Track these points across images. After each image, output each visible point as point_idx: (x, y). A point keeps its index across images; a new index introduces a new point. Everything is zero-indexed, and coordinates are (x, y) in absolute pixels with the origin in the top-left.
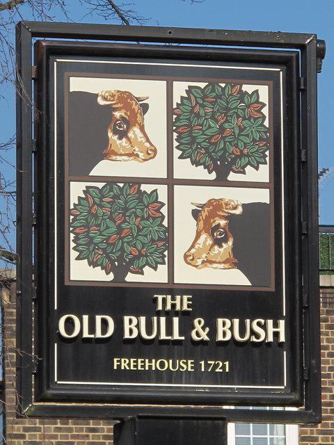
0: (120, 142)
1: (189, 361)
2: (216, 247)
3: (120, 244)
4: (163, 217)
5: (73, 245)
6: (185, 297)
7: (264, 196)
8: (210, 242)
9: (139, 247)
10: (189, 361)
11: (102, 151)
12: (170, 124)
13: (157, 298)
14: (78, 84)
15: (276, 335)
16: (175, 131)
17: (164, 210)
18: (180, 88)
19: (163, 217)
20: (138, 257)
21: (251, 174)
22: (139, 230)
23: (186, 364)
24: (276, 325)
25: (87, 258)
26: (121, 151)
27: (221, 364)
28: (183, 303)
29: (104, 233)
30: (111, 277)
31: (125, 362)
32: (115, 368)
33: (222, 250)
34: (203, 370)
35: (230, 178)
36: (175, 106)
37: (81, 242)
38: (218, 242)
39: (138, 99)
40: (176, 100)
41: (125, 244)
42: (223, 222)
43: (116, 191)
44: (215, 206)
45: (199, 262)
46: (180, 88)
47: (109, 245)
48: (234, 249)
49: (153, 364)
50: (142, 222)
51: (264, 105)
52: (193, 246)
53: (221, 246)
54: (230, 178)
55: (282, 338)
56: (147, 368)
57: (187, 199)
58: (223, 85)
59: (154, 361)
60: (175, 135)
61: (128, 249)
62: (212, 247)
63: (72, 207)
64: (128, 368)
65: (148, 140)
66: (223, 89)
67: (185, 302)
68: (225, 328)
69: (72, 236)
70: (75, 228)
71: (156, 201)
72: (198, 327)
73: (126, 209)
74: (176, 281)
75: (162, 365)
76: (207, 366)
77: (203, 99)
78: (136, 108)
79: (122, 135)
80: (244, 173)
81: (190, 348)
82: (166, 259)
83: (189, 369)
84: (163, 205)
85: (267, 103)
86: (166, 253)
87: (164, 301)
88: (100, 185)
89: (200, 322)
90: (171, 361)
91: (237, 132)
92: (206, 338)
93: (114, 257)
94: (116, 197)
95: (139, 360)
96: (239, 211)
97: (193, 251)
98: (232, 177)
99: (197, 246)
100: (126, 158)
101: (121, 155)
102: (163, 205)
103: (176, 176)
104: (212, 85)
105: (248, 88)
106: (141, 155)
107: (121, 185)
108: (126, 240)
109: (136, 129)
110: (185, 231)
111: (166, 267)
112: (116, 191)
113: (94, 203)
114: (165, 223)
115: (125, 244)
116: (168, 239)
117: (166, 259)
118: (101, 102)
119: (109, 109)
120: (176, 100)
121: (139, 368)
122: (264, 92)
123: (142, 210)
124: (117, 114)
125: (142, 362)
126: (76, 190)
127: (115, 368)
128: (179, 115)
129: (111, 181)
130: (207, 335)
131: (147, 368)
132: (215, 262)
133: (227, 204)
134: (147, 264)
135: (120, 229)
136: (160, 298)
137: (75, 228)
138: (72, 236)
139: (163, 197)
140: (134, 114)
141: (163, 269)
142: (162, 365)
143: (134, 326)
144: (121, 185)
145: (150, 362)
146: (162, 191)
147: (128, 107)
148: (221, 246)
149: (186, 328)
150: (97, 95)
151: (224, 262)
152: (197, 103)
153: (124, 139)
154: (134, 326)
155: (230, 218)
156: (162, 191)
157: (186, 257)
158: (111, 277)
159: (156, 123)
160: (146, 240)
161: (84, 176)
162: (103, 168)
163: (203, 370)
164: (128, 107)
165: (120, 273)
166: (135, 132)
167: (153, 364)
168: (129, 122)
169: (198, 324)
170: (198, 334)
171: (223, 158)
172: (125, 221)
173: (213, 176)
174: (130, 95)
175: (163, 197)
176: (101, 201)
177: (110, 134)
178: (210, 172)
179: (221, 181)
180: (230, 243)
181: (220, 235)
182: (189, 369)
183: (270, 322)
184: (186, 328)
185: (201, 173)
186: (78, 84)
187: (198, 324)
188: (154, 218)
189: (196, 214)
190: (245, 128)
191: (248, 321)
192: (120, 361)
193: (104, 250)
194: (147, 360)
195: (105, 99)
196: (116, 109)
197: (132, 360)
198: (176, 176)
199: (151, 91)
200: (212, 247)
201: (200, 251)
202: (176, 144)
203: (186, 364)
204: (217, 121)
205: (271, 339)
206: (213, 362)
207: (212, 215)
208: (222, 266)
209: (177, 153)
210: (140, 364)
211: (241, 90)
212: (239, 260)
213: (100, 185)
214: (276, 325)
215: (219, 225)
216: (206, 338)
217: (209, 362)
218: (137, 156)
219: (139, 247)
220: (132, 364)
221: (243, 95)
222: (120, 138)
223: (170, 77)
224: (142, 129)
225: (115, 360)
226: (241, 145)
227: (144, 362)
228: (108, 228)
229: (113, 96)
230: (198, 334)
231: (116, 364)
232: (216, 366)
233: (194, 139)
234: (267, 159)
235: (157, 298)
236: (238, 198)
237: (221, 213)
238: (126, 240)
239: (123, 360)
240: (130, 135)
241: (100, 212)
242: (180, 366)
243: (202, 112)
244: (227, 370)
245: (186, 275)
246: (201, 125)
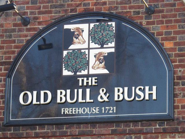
0: (76, 40)
1: (97, 108)
3: (76, 65)
4: (87, 58)
5: (64, 66)
6: (94, 78)
7: (113, 50)
8: (99, 63)
9: (80, 66)
10: (97, 108)
11: (71, 42)
12: (89, 34)
13: (163, 43)
15: (150, 95)
16: (90, 36)
17: (87, 56)
19: (87, 58)
20: (80, 68)
21: (110, 45)
22: (81, 61)
23: (95, 109)
24: (151, 89)
25: (67, 69)
26: (77, 42)
27: (112, 108)
28: (93, 81)
29: (72, 63)
30: (73, 74)
31: (67, 110)
32: (62, 113)
33: (102, 65)
34: (103, 112)
35: (104, 46)
36: (90, 30)
37: (66, 66)
38: (101, 63)
39: (81, 29)
40: (91, 28)
41: (77, 65)
42: (102, 58)
43: (75, 52)
44: (100, 54)
45: (96, 68)
46: (92, 25)
47: (73, 66)
48: (105, 64)
49: (80, 110)
50: (81, 60)
51: (114, 27)
52: (94, 64)
53: (101, 64)
54: (104, 46)
55: (154, 97)
56: (77, 113)
57: (93, 53)
58: (103, 23)
59: (80, 108)
60: (90, 37)
61: (78, 66)
62: (99, 64)
63: (64, 57)
64: (68, 113)
65: (83, 39)
66: (103, 24)
67: (94, 81)
68: (119, 94)
69: (64, 64)
70: (64, 62)
71: (85, 54)
72: (102, 94)
73: (77, 57)
74: (90, 73)
75: (84, 111)
76: (105, 110)
77: (98, 27)
78: (81, 31)
79: (77, 38)
80: (108, 45)
82: (87, 68)
83: (97, 112)
84: (87, 55)
85: (114, 26)
86: (87, 67)
87: (83, 80)
88: (71, 51)
89: (103, 90)
90: (88, 108)
91: (106, 34)
92: (106, 100)
93: (74, 69)
94: (75, 54)
95: (74, 109)
96: (106, 55)
97: (94, 66)
98: (105, 46)
99: (95, 64)
100: (78, 44)
101: (77, 43)
102: (87, 55)
103: (90, 47)
104: (100, 23)
105: (110, 23)
106: (82, 43)
107: (76, 51)
108: (77, 64)
109: (81, 36)
110: (92, 60)
111: (87, 70)
112: (75, 52)
113: (70, 56)
114: (87, 59)
115: (77, 65)
116: (88, 64)
117: (87, 68)
118: (72, 30)
119: (74, 32)
120: (91, 28)
121: (73, 113)
122: (114, 24)
123: (81, 56)
124: (76, 33)
125: (75, 109)
126: (65, 53)
127: (62, 113)
128: (91, 32)
129: (74, 50)
130: (107, 98)
131: (77, 113)
132: (100, 68)
133: (103, 53)
134: (82, 70)
135: (76, 62)
136: (80, 79)
137: (64, 62)
138: (64, 64)
139: (87, 53)
140: (80, 33)
141: (86, 71)
142: (84, 111)
144: (76, 51)
145: (79, 109)
146: (87, 51)
147: (79, 31)
148: (101, 64)
149: (94, 94)
150: (71, 29)
151: (102, 68)
152: (96, 28)
153: (77, 39)
155: (104, 56)
156: (87, 51)
157: (92, 67)
158: (73, 74)
159: (85, 35)
160: (82, 64)
161: (67, 49)
162: (72, 47)
163: (103, 112)
164: (79, 31)
165: (75, 73)
166: (80, 37)
167: (80, 110)
168: (78, 35)
170: (101, 97)
171: (103, 42)
172: (77, 60)
173: (100, 46)
174: (79, 28)
175: (87, 53)
176: (71, 55)
177: (74, 38)
178: (99, 45)
179: (102, 47)
180: (104, 63)
181: (101, 61)
182: (97, 112)
183: (147, 88)
185: (97, 46)
188: (84, 58)
189: (95, 56)
190: (109, 33)
191: (133, 88)
192: (64, 110)
193: (71, 67)
194: (77, 109)
195: (73, 30)
196: (75, 32)
197: (70, 109)
198: (90, 47)
199: (85, 27)
200: (99, 64)
201: (96, 65)
202: (90, 39)
203: (95, 109)
204: (101, 32)
205: (147, 98)
206: (108, 108)
207: (100, 56)
208: (102, 69)
209: (91, 41)
210: (74, 111)
211: (108, 24)
212: (106, 67)
213: (71, 51)
214: (151, 89)
215: (101, 58)
216: (106, 100)
217: (106, 108)
218: (81, 43)
219: (80, 66)
220: (70, 111)
221: (108, 25)
222: (76, 39)
223: (88, 22)
224: (82, 36)
225: (62, 109)
226: (107, 37)
227: (75, 109)
228: (73, 61)
229: (75, 29)
230: (101, 97)
231: (62, 111)
232: (109, 110)
233: (95, 37)
234: (114, 41)
235: (79, 80)
236: (106, 51)
237: (102, 55)
238: (77, 64)
239: (66, 109)
240: (79, 38)
241: (71, 58)
242: (93, 111)
243: (97, 31)
244: (115, 112)
246: (97, 34)
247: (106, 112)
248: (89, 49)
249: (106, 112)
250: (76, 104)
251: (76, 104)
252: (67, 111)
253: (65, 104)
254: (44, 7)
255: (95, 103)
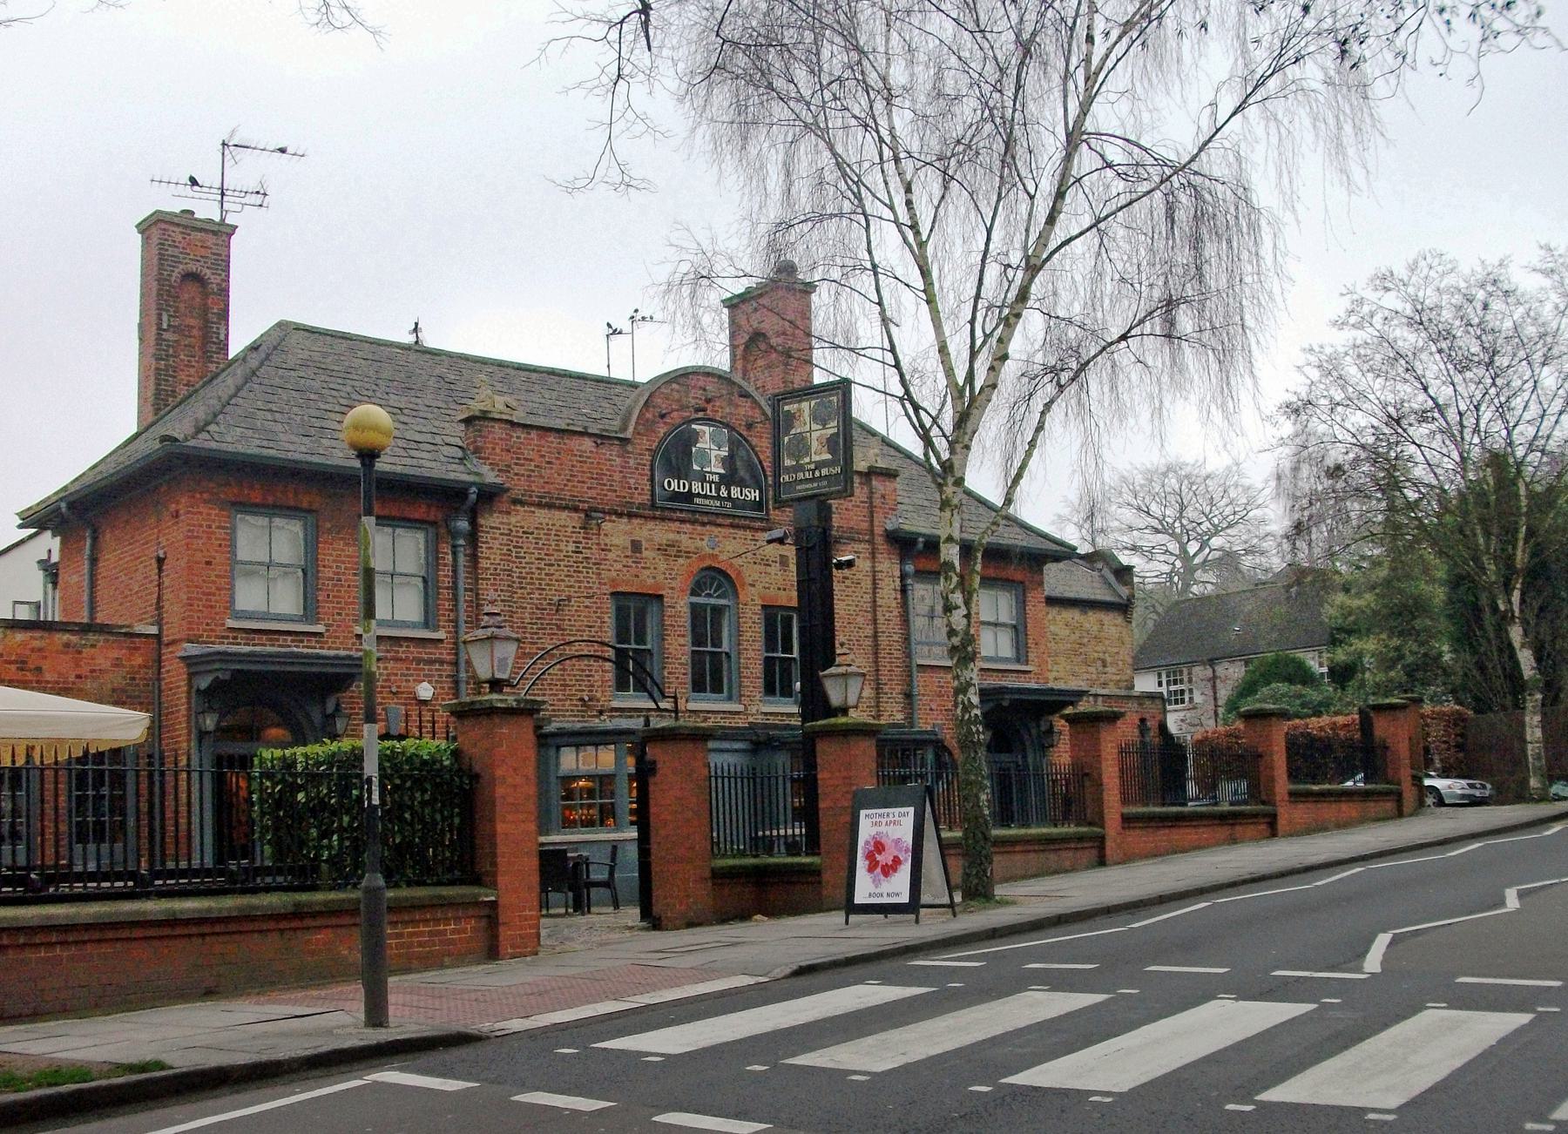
2: (162, 556)
14: (786, 408)
18: (813, 403)
21: (832, 424)
28: (813, 467)
46: (813, 403)
57: (815, 435)
81: (813, 480)
103: (398, 570)
110: (815, 445)
126: (786, 439)
143: (801, 476)
149: (718, 490)
154: (801, 476)
161: (787, 434)
162: (793, 432)
169: (723, 489)
179: (824, 428)
184: (718, 490)
186: (786, 408)
187: (723, 489)
245: (816, 458)
247: (1529, 1126)
248: (810, 431)
249: (1529, 1126)
250: (705, 496)
251: (705, 496)
252: (697, 500)
253: (699, 495)
254: (408, 681)
255: (718, 498)
